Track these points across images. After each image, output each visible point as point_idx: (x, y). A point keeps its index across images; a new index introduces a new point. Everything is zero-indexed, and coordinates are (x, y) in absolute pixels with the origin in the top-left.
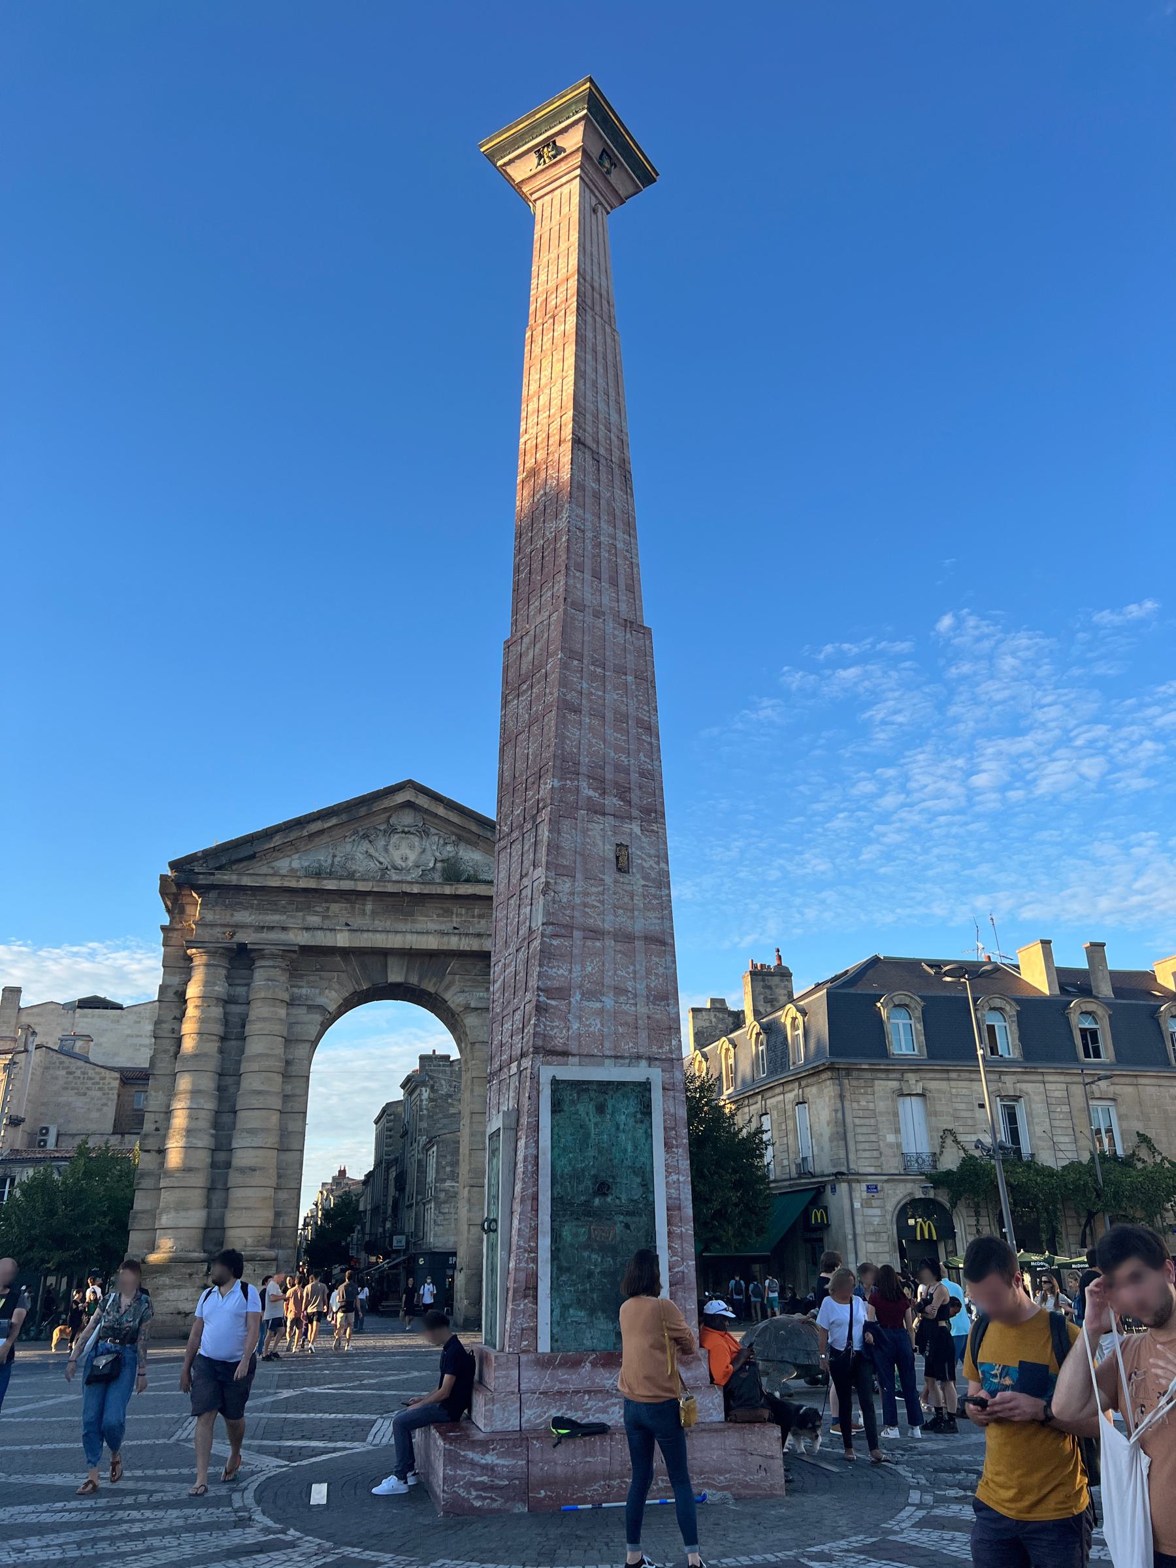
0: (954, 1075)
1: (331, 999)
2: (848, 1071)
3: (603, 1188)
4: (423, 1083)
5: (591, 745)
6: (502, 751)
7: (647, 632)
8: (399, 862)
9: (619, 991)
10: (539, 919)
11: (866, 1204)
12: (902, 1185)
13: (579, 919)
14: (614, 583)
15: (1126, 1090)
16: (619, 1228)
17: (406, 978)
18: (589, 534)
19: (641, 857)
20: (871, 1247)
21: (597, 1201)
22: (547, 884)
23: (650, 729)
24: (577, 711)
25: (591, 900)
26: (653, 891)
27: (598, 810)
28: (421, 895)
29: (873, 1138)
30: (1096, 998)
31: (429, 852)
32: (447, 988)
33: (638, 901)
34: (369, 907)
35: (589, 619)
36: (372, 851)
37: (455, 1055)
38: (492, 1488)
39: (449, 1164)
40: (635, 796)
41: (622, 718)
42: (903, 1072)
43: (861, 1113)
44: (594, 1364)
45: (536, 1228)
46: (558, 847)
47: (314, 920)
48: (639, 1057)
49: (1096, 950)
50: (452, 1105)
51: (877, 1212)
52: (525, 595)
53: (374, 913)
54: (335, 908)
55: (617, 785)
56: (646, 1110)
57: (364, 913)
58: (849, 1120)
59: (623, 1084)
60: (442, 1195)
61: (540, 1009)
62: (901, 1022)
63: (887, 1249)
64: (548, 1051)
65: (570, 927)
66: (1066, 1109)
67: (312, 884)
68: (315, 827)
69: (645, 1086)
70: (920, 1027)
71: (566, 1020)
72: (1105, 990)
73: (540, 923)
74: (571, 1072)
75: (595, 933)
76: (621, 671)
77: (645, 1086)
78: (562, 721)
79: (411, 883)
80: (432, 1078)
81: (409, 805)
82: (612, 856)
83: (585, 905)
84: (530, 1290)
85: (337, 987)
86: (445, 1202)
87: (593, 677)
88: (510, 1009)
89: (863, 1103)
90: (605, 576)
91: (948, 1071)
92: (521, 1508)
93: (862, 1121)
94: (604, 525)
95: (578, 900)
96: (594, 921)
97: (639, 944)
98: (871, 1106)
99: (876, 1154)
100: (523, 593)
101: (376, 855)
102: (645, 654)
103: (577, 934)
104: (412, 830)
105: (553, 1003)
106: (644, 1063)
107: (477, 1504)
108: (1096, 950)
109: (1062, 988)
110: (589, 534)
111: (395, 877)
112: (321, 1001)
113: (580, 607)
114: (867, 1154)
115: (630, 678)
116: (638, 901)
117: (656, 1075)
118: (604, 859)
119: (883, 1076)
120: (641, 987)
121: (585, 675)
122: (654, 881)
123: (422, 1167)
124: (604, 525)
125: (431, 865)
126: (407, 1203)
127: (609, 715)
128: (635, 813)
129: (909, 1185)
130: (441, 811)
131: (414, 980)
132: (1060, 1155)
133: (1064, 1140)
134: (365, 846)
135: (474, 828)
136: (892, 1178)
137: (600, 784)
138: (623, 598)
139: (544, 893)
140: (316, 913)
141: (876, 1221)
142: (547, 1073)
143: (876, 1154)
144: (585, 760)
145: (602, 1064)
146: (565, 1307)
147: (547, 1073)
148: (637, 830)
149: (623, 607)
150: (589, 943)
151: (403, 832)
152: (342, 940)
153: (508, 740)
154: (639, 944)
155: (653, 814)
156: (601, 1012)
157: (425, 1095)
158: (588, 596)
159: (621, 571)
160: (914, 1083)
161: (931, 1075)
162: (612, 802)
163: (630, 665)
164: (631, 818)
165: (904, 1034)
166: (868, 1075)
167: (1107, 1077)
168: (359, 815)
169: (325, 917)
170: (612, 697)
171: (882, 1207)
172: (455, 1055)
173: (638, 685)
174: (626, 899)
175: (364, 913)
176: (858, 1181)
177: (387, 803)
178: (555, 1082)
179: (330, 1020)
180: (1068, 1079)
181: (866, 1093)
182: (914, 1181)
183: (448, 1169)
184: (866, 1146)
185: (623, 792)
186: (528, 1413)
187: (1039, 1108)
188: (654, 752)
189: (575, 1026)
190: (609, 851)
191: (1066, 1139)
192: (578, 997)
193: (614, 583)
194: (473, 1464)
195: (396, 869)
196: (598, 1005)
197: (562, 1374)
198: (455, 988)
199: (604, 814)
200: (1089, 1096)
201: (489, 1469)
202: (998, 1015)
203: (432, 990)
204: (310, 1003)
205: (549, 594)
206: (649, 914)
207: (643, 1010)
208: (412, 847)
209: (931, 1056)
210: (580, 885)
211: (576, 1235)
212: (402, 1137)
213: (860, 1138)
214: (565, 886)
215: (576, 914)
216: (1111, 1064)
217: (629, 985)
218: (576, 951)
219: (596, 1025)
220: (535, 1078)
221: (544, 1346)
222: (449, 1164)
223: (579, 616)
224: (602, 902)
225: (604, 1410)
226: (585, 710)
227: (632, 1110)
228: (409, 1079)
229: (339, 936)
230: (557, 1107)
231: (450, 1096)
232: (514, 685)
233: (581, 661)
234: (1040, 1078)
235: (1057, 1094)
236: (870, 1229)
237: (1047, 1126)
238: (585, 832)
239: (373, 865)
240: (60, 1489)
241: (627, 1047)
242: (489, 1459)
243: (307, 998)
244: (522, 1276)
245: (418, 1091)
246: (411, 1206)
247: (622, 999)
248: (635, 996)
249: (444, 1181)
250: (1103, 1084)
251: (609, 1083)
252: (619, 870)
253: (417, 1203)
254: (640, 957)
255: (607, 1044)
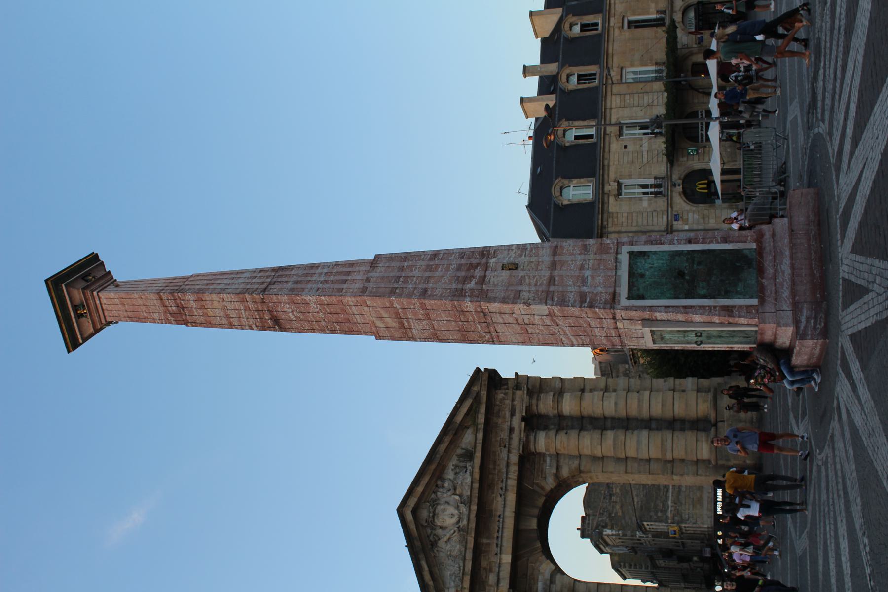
0: (606, 162)
1: (546, 569)
2: (603, 227)
3: (681, 274)
4: (601, 534)
5: (446, 283)
6: (441, 341)
7: (377, 257)
8: (454, 520)
9: (582, 268)
10: (544, 309)
11: (686, 222)
12: (674, 199)
13: (544, 288)
14: (349, 273)
15: (616, 61)
16: (700, 267)
17: (533, 516)
18: (320, 286)
19: (511, 258)
20: (712, 221)
21: (687, 278)
22: (524, 303)
23: (435, 254)
24: (426, 290)
25: (533, 282)
26: (528, 252)
27: (482, 280)
28: (479, 505)
29: (645, 215)
30: (558, 73)
31: (447, 499)
32: (542, 488)
33: (534, 259)
34: (485, 541)
35: (371, 285)
36: (446, 539)
37: (586, 485)
38: (816, 318)
39: (656, 514)
40: (474, 261)
41: (429, 268)
42: (603, 193)
43: (630, 221)
44: (762, 278)
45: (700, 307)
46: (504, 298)
47: (492, 578)
48: (616, 258)
49: (527, 71)
50: (616, 513)
51: (690, 215)
52: (350, 325)
53: (488, 538)
54: (484, 564)
55: (468, 270)
56: (643, 254)
57: (488, 544)
58: (634, 229)
59: (630, 264)
60: (676, 518)
61: (591, 306)
62: (572, 193)
63: (713, 211)
64: (614, 298)
65: (548, 292)
66: (627, 97)
67: (467, 579)
68: (427, 577)
69: (631, 254)
70: (575, 181)
71: (597, 294)
72: (553, 68)
73: (545, 307)
74: (623, 290)
75: (551, 280)
76: (401, 269)
77: (631, 254)
78: (432, 297)
79: (470, 510)
80: (597, 528)
81: (415, 512)
82: (509, 272)
83: (536, 285)
84: (728, 310)
85: (538, 564)
86: (681, 517)
87: (406, 281)
88: (588, 329)
89: (624, 219)
90: (345, 278)
91: (604, 166)
92: (824, 305)
93: (635, 221)
94: (314, 278)
95: (533, 288)
96: (545, 280)
97: (557, 259)
98: (625, 215)
99: (655, 214)
100: (349, 327)
101: (448, 536)
102: (391, 257)
103: (552, 288)
104: (432, 510)
105: (588, 300)
106: (619, 256)
107: (823, 324)
108: (527, 71)
109: (552, 93)
110: (320, 286)
111: (465, 522)
112: (547, 575)
113: (364, 290)
114: (655, 219)
115: (406, 264)
116: (534, 259)
117: (625, 249)
118: (511, 276)
119: (606, 206)
120: (579, 258)
121: (404, 286)
122: (522, 251)
123: (657, 535)
124: (314, 278)
125: (457, 497)
126: (681, 548)
127: (427, 274)
128: (484, 261)
129: (675, 194)
130: (420, 489)
131: (537, 509)
132: (655, 102)
133: (647, 99)
134: (441, 543)
135: (433, 467)
136: (670, 204)
137: (466, 279)
138: (357, 269)
139: (529, 305)
140: (487, 577)
141: (696, 216)
142: (624, 302)
143: (655, 214)
144: (454, 286)
145: (620, 276)
146: (737, 292)
147: (624, 302)
148: (494, 260)
149: (362, 269)
150: (556, 283)
151: (433, 516)
152: (507, 558)
153: (436, 337)
154: (557, 259)
155: (485, 253)
156: (593, 277)
157: (609, 532)
158: (357, 286)
159: (341, 270)
160: (611, 187)
161: (606, 176)
162: (478, 273)
163: (398, 264)
164: (487, 263)
165: (578, 192)
166: (606, 215)
167: (609, 71)
168: (421, 543)
169: (491, 571)
170: (417, 273)
171: (688, 212)
172: (586, 485)
173: (409, 260)
174: (533, 265)
175: (488, 544)
176: (672, 226)
177: (413, 527)
178: (629, 298)
179: (558, 570)
180: (609, 94)
181: (617, 217)
182: (672, 192)
183: (659, 514)
184: (650, 219)
185: (473, 267)
186: (785, 307)
187: (627, 112)
188: (448, 253)
189: (600, 289)
190: (506, 274)
191: (646, 98)
192: (585, 288)
193: (349, 273)
194: (806, 327)
195: (458, 522)
196: (589, 278)
197: (767, 293)
198: (543, 484)
199: (485, 276)
200: (620, 82)
201: (808, 319)
202: (567, 133)
203: (542, 500)
204: (548, 582)
205: (354, 308)
206: (541, 253)
207: (591, 257)
208: (444, 510)
209: (593, 175)
210: (525, 288)
211: (703, 288)
212: (636, 553)
213: (645, 222)
214: (525, 295)
215: (540, 289)
216: (600, 67)
217: (579, 263)
218: (561, 289)
219: (600, 279)
220: (627, 308)
221: (755, 302)
222: (656, 514)
223: (370, 289)
224: (534, 277)
225: (783, 272)
226: (424, 286)
227: (643, 262)
228: (597, 546)
229: (504, 561)
230: (641, 297)
231: (610, 514)
232: (404, 334)
233: (396, 288)
234: (608, 111)
235: (618, 101)
236: (701, 221)
237: (639, 109)
238: (495, 285)
239: (456, 537)
240: (824, 560)
241: (611, 264)
242: (803, 319)
243: (545, 584)
244: (722, 313)
245: (606, 537)
246: (683, 543)
247: (586, 266)
248: (584, 260)
249: (667, 517)
250: (613, 73)
251: (629, 272)
252: (516, 268)
253: (682, 538)
254: (564, 258)
255: (610, 273)
